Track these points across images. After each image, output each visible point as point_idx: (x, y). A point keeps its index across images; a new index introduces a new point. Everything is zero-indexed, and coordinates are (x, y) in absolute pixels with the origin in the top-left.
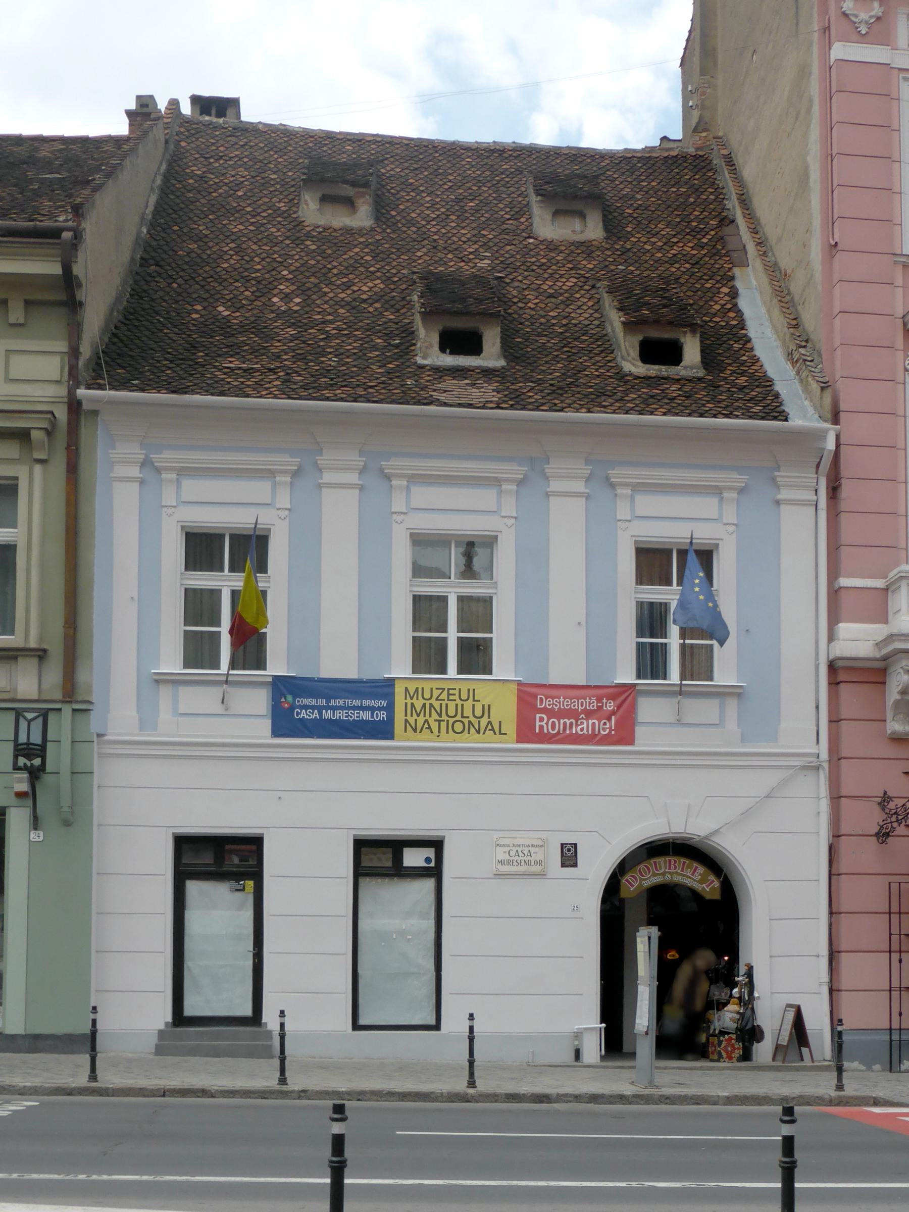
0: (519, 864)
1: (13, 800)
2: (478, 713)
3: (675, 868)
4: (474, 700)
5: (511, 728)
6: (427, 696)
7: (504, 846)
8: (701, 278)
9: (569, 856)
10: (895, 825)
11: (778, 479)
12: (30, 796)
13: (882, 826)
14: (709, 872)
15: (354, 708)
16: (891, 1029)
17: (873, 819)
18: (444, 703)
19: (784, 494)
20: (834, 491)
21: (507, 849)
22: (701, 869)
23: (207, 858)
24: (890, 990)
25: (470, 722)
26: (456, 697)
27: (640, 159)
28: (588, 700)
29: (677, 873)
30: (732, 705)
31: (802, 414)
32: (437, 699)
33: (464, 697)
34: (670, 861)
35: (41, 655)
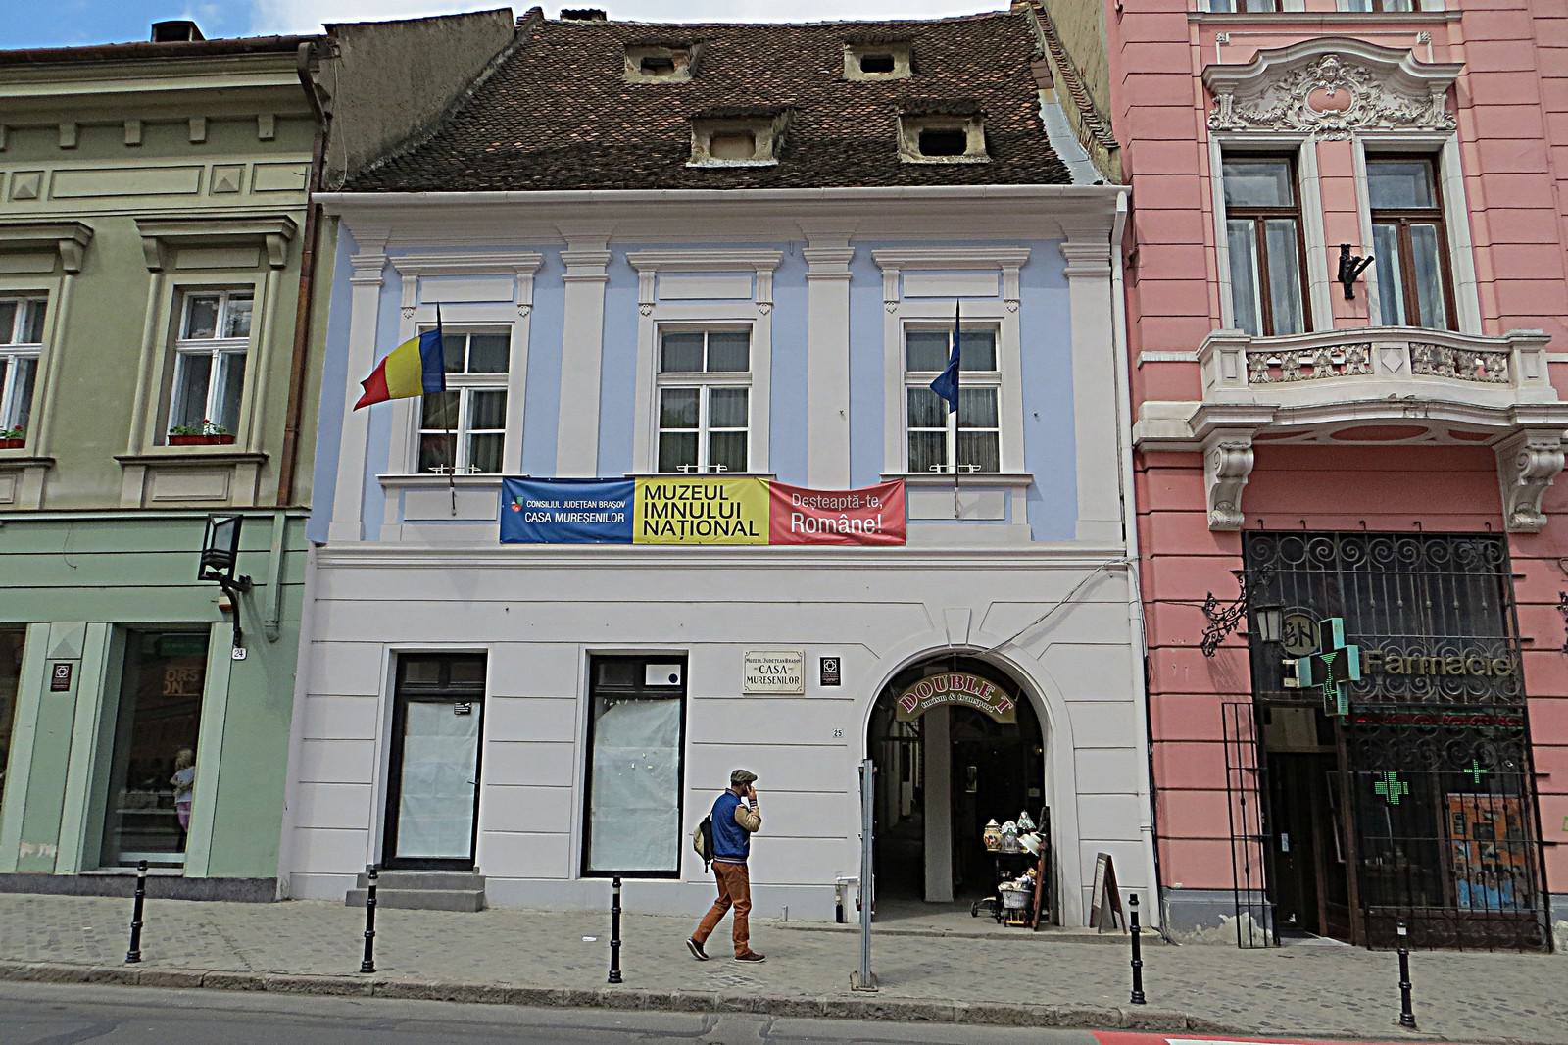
0: (772, 681)
1: (220, 615)
2: (726, 512)
3: (961, 686)
4: (722, 498)
5: (763, 530)
6: (670, 494)
7: (755, 661)
8: (1003, 98)
9: (831, 674)
10: (1223, 632)
11: (1066, 251)
12: (232, 610)
13: (1207, 635)
14: (1000, 690)
15: (590, 510)
16: (1236, 890)
17: (1197, 627)
18: (688, 503)
19: (1072, 267)
20: (1131, 263)
21: (758, 665)
22: (992, 688)
23: (431, 681)
24: (1232, 840)
25: (717, 523)
26: (702, 495)
27: (957, 23)
28: (849, 499)
29: (963, 692)
30: (1019, 500)
31: (1084, 174)
32: (681, 498)
33: (711, 494)
34: (954, 678)
35: (261, 461)
